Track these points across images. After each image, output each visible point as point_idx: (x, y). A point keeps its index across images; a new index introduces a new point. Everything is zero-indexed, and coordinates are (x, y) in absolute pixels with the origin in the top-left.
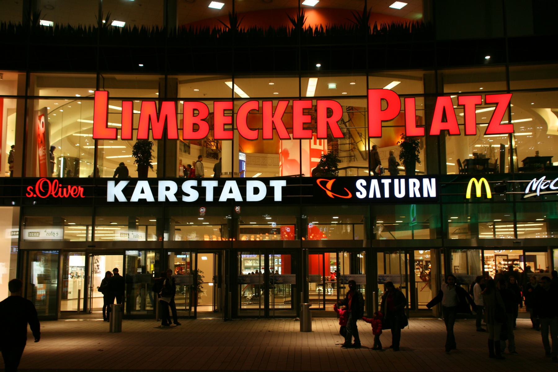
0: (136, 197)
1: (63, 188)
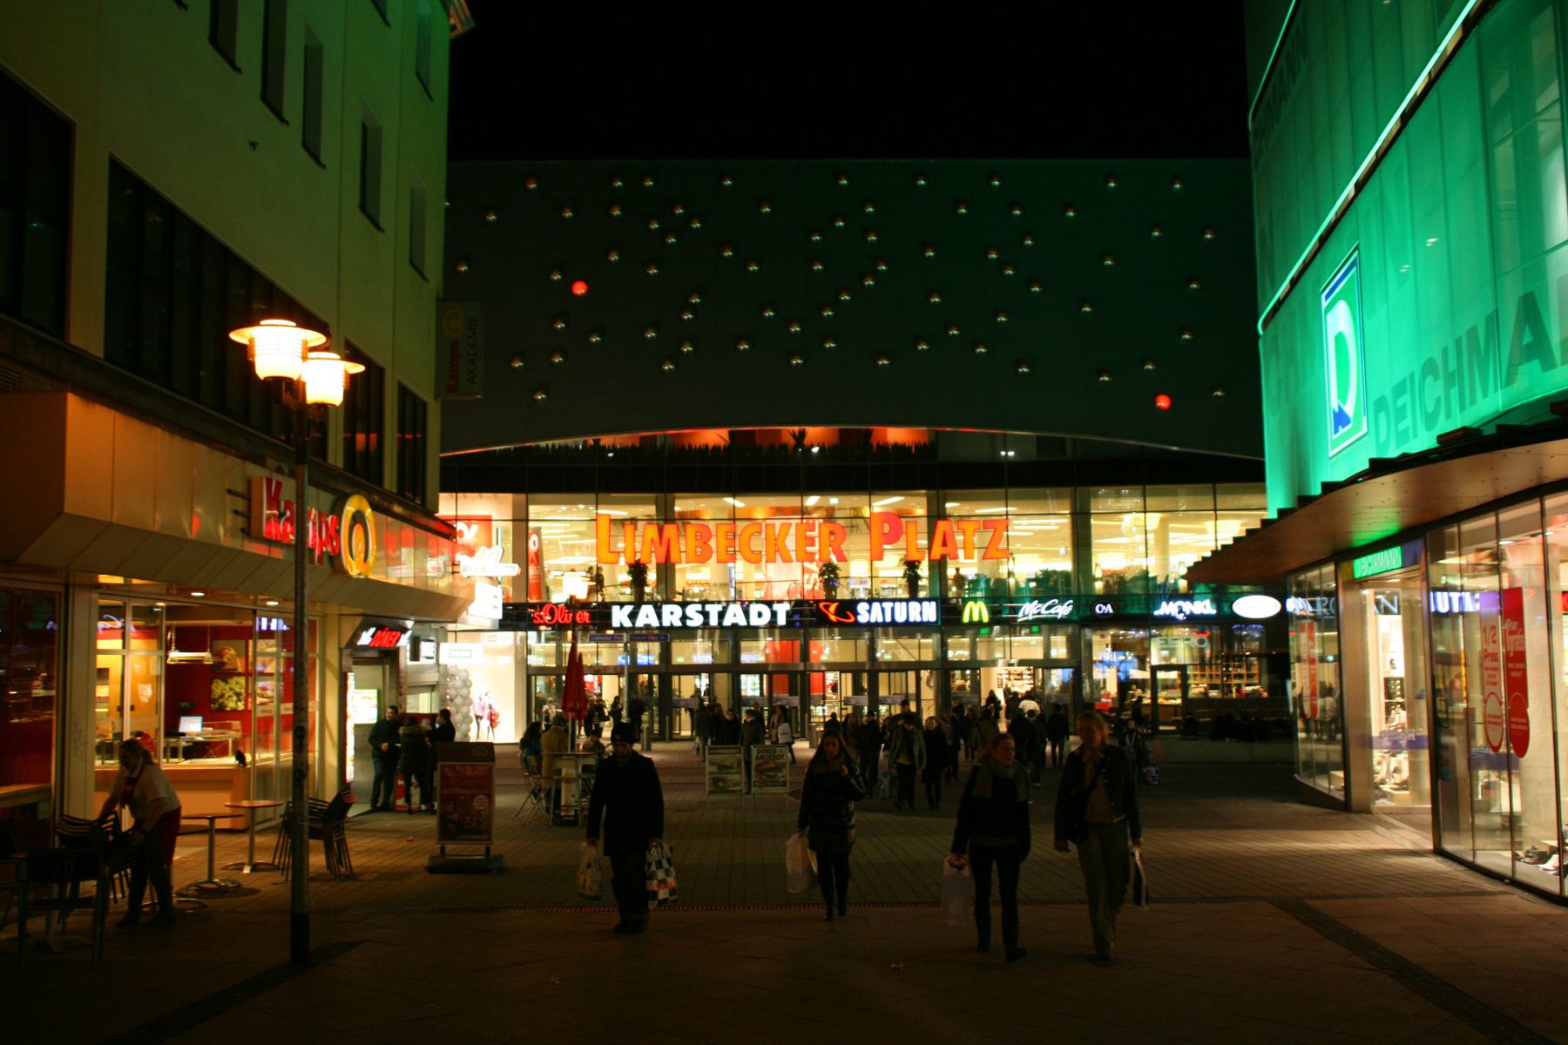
0: (640, 623)
1: (569, 613)
